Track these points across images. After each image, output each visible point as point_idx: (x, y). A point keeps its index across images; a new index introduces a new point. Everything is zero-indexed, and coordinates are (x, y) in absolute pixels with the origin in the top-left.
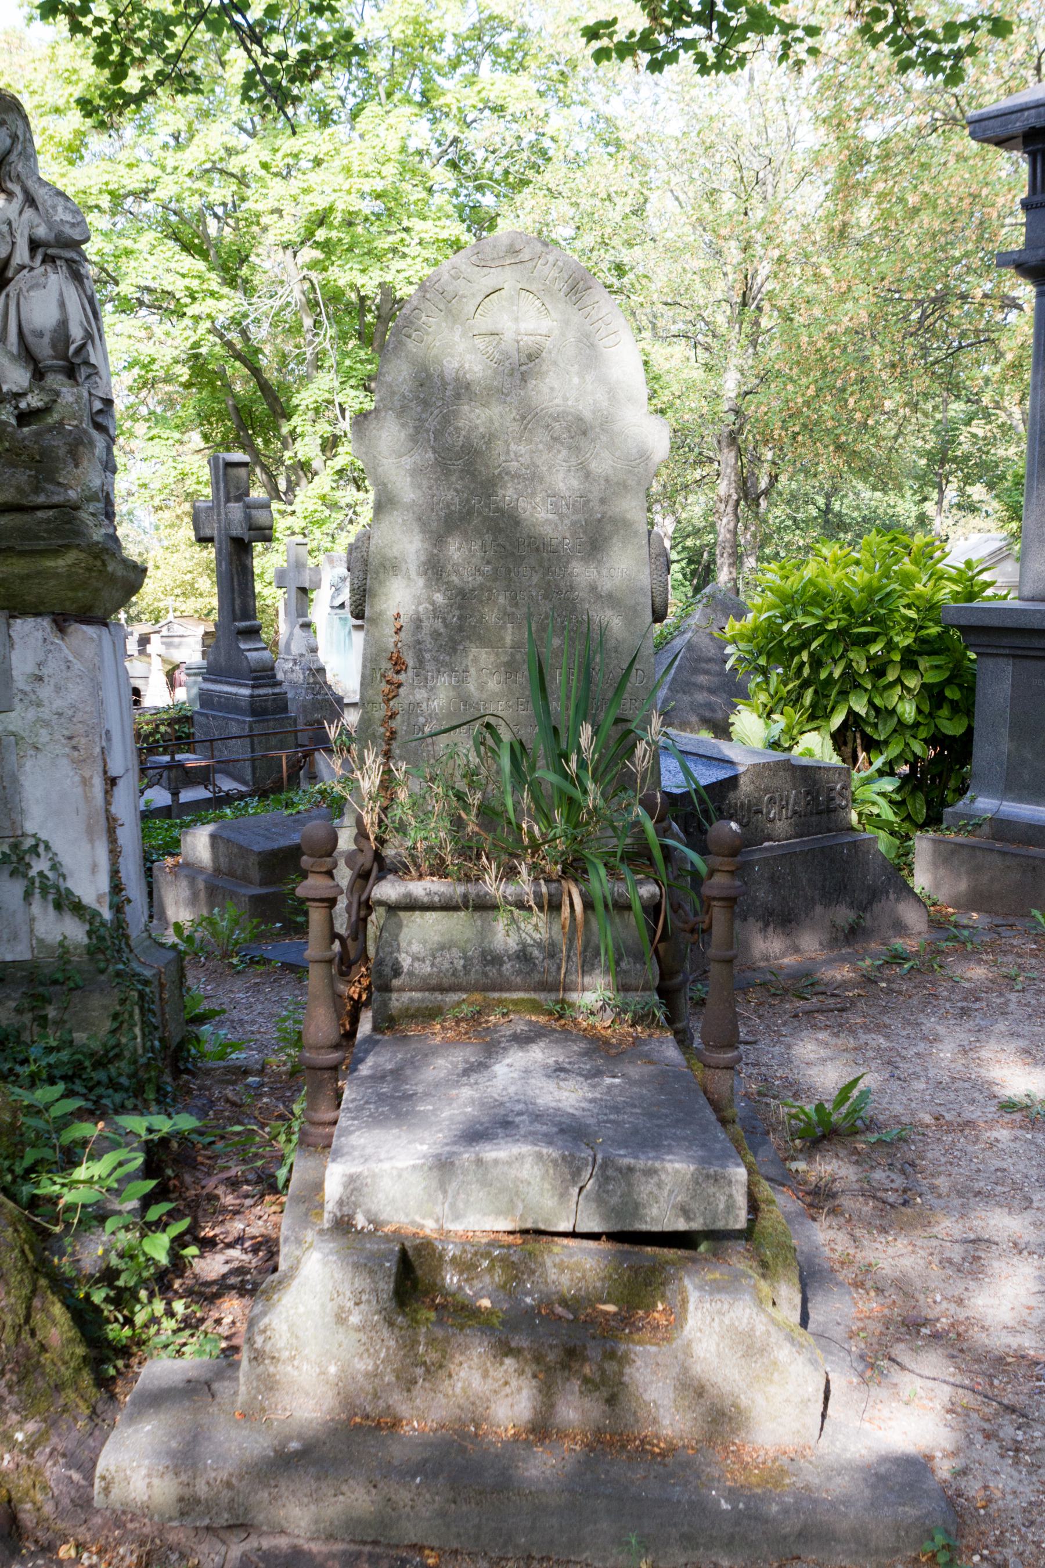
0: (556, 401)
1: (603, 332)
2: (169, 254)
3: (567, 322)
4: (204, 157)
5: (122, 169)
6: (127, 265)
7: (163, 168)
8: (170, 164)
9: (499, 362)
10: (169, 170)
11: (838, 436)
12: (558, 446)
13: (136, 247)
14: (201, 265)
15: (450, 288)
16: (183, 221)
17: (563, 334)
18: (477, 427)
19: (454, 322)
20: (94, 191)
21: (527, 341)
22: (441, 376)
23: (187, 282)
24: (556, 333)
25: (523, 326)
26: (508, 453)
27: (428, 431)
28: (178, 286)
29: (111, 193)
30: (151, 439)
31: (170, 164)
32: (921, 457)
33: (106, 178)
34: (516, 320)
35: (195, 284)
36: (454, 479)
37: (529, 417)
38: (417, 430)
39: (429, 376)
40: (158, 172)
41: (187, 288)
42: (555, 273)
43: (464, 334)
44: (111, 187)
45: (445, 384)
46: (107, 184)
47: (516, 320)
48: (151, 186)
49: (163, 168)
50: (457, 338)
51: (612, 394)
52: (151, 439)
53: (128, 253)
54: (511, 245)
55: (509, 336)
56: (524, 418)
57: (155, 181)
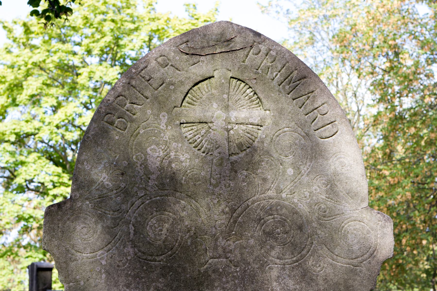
0: (270, 193)
1: (319, 122)
2: (44, 164)
3: (281, 112)
4: (64, 117)
5: (23, 123)
6: (21, 169)
7: (43, 122)
8: (47, 121)
9: (207, 152)
10: (46, 123)
11: (397, 260)
12: (271, 242)
13: (27, 160)
14: (59, 170)
15: (157, 75)
16: (56, 151)
17: (276, 124)
18: (182, 220)
19: (161, 109)
20: (8, 133)
21: (239, 131)
22: (145, 164)
23: (52, 178)
24: (269, 121)
25: (234, 115)
26: (216, 248)
27: (128, 223)
28: (47, 180)
29: (16, 134)
30: (27, 257)
31: (47, 121)
32: (423, 273)
33: (14, 126)
34: (227, 108)
35: (56, 179)
36: (153, 276)
37: (239, 215)
38: (116, 222)
39: (131, 165)
40: (41, 124)
41: (52, 181)
42: (267, 62)
43: (170, 122)
44: (16, 131)
45: (148, 173)
46: (14, 129)
47: (227, 108)
48: (37, 131)
49: (43, 122)
50: (163, 126)
51: (331, 186)
52: (27, 257)
53: (23, 163)
54: (222, 34)
55: (219, 124)
56: (233, 211)
57: (39, 129)
